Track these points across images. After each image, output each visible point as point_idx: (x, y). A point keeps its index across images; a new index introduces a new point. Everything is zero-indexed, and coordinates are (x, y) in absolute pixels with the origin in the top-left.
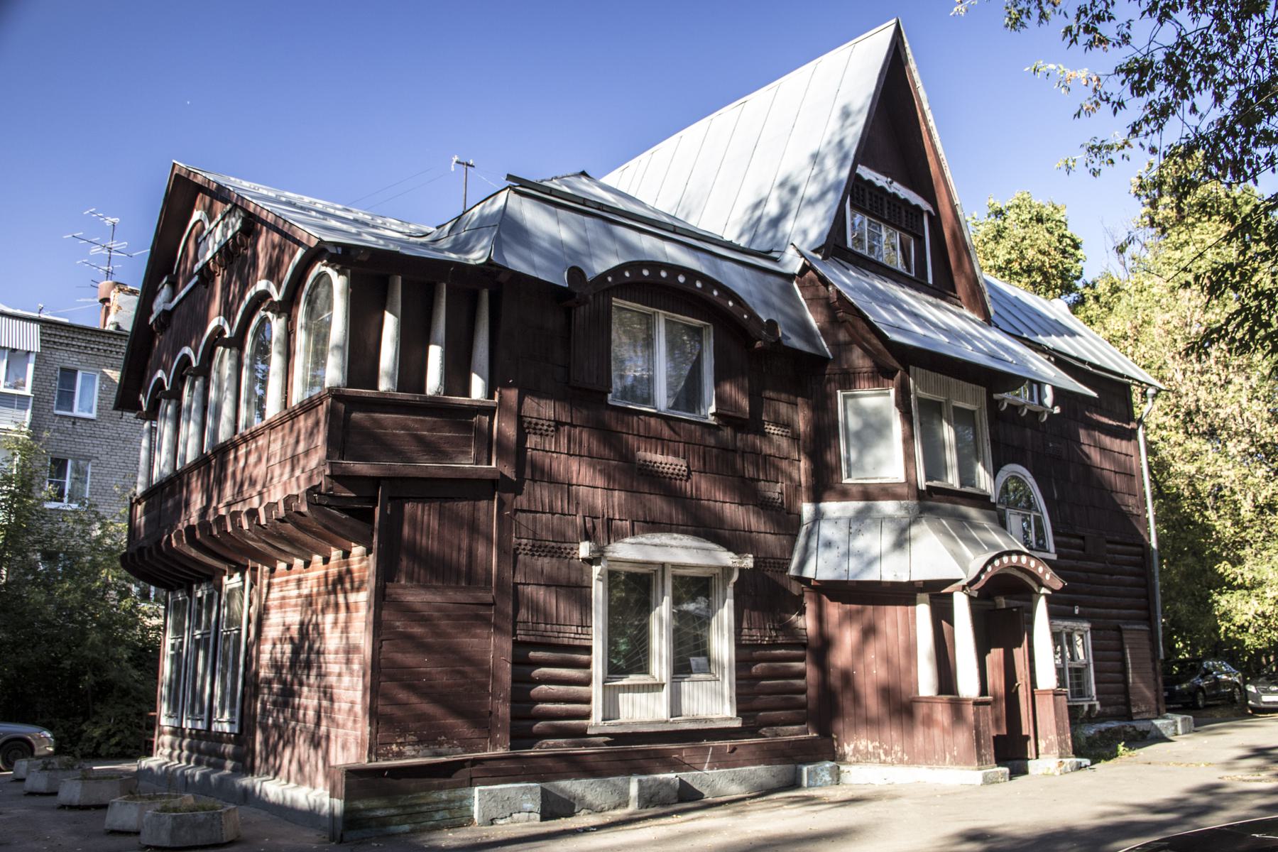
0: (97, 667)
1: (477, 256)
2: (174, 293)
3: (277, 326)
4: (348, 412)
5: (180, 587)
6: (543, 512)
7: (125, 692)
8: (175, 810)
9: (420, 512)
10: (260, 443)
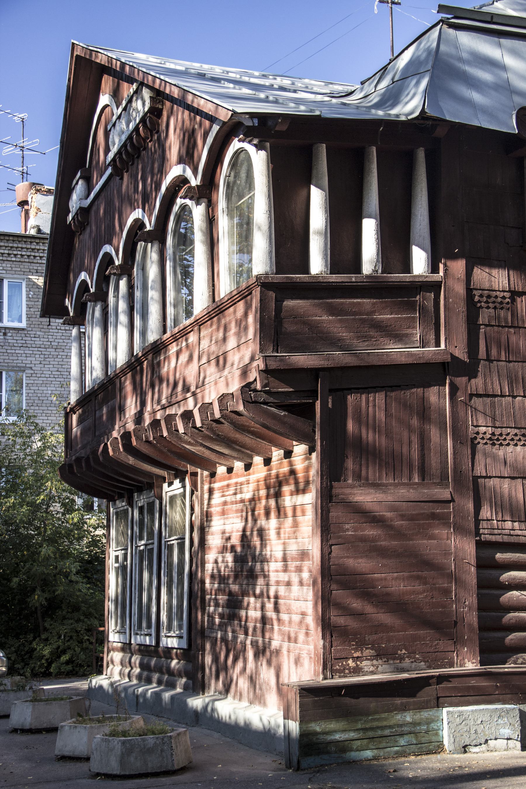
0: (46, 583)
1: (410, 106)
2: (89, 188)
3: (198, 212)
4: (279, 302)
5: (121, 497)
6: (502, 396)
7: (76, 608)
8: (124, 734)
9: (364, 404)
10: (190, 340)
